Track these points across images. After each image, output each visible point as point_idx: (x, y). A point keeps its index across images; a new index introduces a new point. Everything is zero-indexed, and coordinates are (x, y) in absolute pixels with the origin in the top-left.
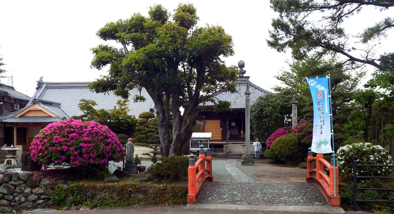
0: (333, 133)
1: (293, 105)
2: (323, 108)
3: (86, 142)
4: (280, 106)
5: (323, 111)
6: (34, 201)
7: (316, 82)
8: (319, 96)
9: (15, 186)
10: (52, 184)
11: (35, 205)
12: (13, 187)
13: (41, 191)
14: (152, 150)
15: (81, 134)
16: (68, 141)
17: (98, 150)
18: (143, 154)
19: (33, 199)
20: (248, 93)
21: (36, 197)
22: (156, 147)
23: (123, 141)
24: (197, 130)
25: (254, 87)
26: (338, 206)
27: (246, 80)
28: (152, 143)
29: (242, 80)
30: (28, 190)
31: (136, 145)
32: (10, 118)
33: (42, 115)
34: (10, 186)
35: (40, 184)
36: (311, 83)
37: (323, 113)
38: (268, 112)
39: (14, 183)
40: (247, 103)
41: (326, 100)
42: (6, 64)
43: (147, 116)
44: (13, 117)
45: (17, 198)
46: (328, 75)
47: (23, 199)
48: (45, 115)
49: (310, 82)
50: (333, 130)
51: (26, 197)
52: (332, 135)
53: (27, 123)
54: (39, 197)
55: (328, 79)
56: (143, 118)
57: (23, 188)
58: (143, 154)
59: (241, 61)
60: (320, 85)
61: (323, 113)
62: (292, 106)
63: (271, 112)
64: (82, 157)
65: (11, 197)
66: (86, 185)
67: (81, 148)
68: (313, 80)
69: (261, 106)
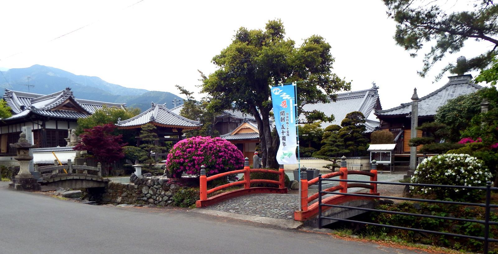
0: (298, 145)
1: (482, 107)
2: (287, 117)
3: (199, 155)
4: (466, 109)
5: (288, 121)
6: (166, 201)
7: (282, 90)
8: (284, 105)
9: (157, 189)
10: (176, 189)
11: (167, 204)
12: (156, 190)
13: (170, 194)
14: (332, 163)
15: (197, 149)
16: (186, 155)
17: (208, 162)
18: (323, 167)
19: (165, 200)
20: (415, 97)
21: (167, 198)
22: (335, 160)
23: (309, 154)
24: (385, 142)
25: (474, 87)
26: (300, 221)
27: (465, 79)
28: (332, 156)
29: (460, 79)
30: (163, 193)
31: (316, 157)
32: (228, 136)
33: (251, 132)
34: (154, 189)
35: (170, 188)
36: (275, 92)
37: (287, 123)
38: (450, 117)
39: (156, 187)
40: (414, 109)
41: (291, 109)
42: (352, 81)
43: (331, 129)
44: (230, 135)
45: (158, 198)
46: (294, 82)
47: (161, 199)
48: (253, 132)
49: (274, 90)
50: (298, 142)
51: (162, 198)
52: (297, 147)
53: (244, 139)
54: (169, 198)
55: (295, 86)
56: (328, 131)
57: (161, 191)
58: (323, 167)
59: (462, 57)
60: (285, 93)
61: (287, 123)
62: (481, 108)
63: (455, 118)
64: (194, 167)
65: (155, 197)
66: (195, 191)
67: (194, 160)
68: (278, 89)
69: (445, 111)
